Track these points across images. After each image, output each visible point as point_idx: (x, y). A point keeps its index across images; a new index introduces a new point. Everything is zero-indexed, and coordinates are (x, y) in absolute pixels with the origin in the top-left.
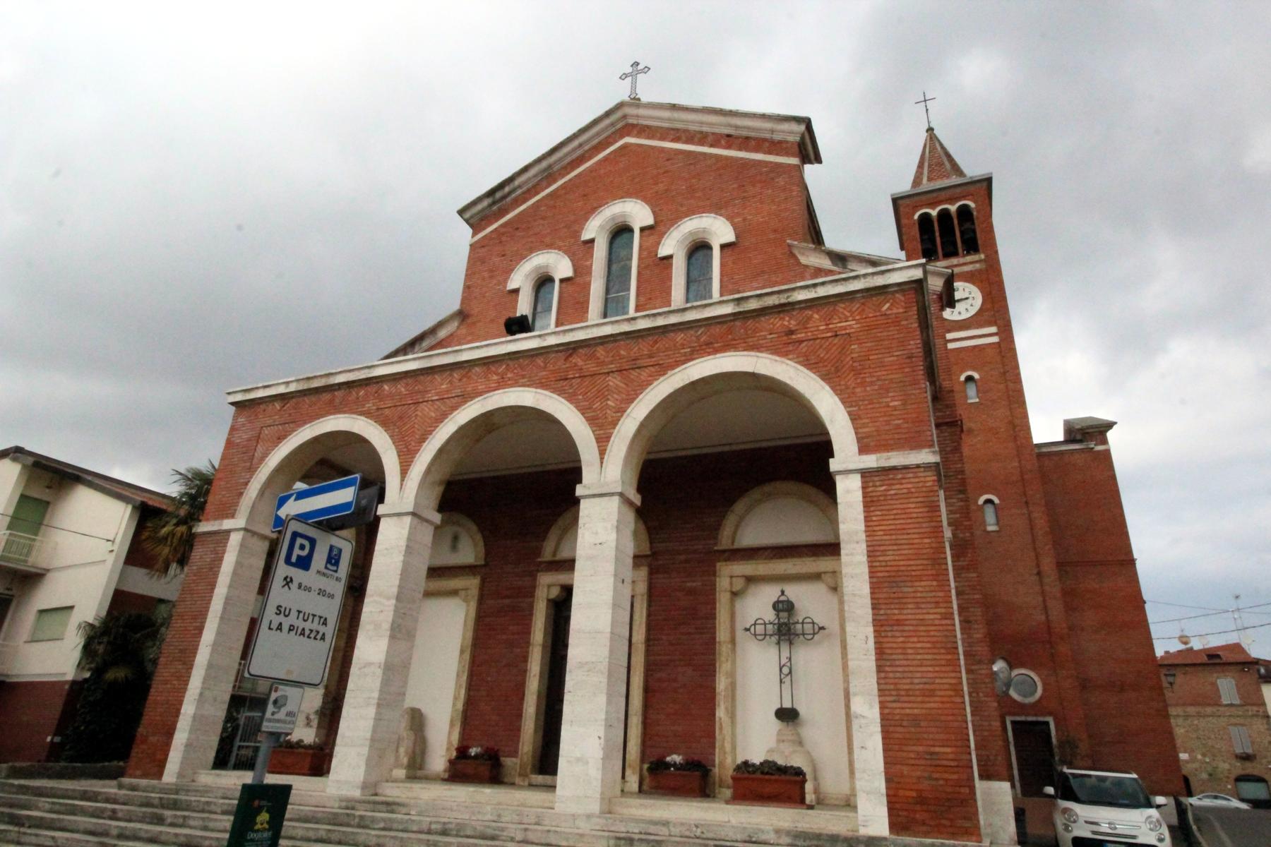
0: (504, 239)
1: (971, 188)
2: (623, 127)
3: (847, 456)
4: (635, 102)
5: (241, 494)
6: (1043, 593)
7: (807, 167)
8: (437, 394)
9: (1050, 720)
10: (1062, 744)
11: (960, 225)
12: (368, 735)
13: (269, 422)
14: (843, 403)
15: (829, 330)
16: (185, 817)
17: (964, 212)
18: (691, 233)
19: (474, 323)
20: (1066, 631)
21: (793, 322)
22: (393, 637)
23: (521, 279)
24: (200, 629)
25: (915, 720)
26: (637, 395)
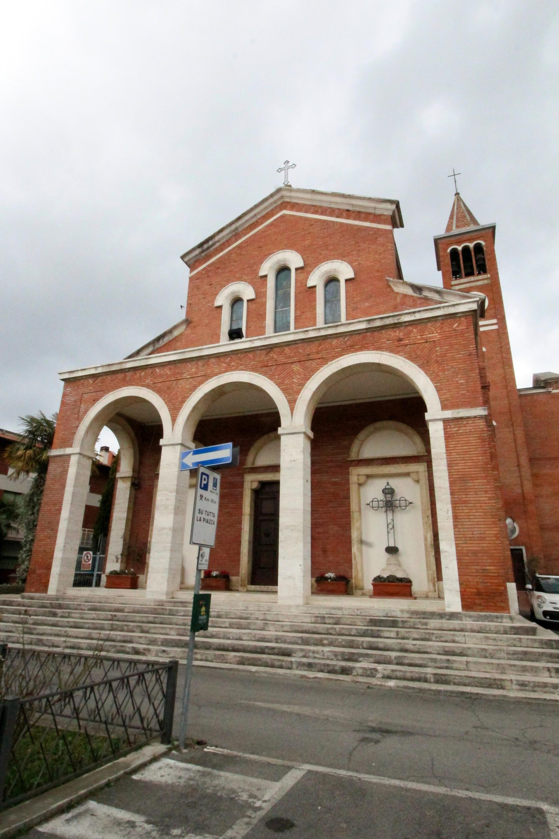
0: (210, 274)
1: (483, 232)
2: (282, 204)
3: (435, 412)
4: (288, 187)
5: (75, 433)
6: (520, 477)
7: (396, 231)
8: (189, 375)
9: (523, 548)
10: (530, 562)
11: (476, 256)
12: (167, 567)
13: (87, 391)
14: (432, 380)
15: (422, 339)
16: (69, 613)
17: (478, 248)
18: (327, 272)
19: (195, 327)
20: (533, 498)
21: (401, 334)
22: (176, 514)
23: (223, 299)
24: (60, 510)
25: (475, 553)
26: (311, 376)
